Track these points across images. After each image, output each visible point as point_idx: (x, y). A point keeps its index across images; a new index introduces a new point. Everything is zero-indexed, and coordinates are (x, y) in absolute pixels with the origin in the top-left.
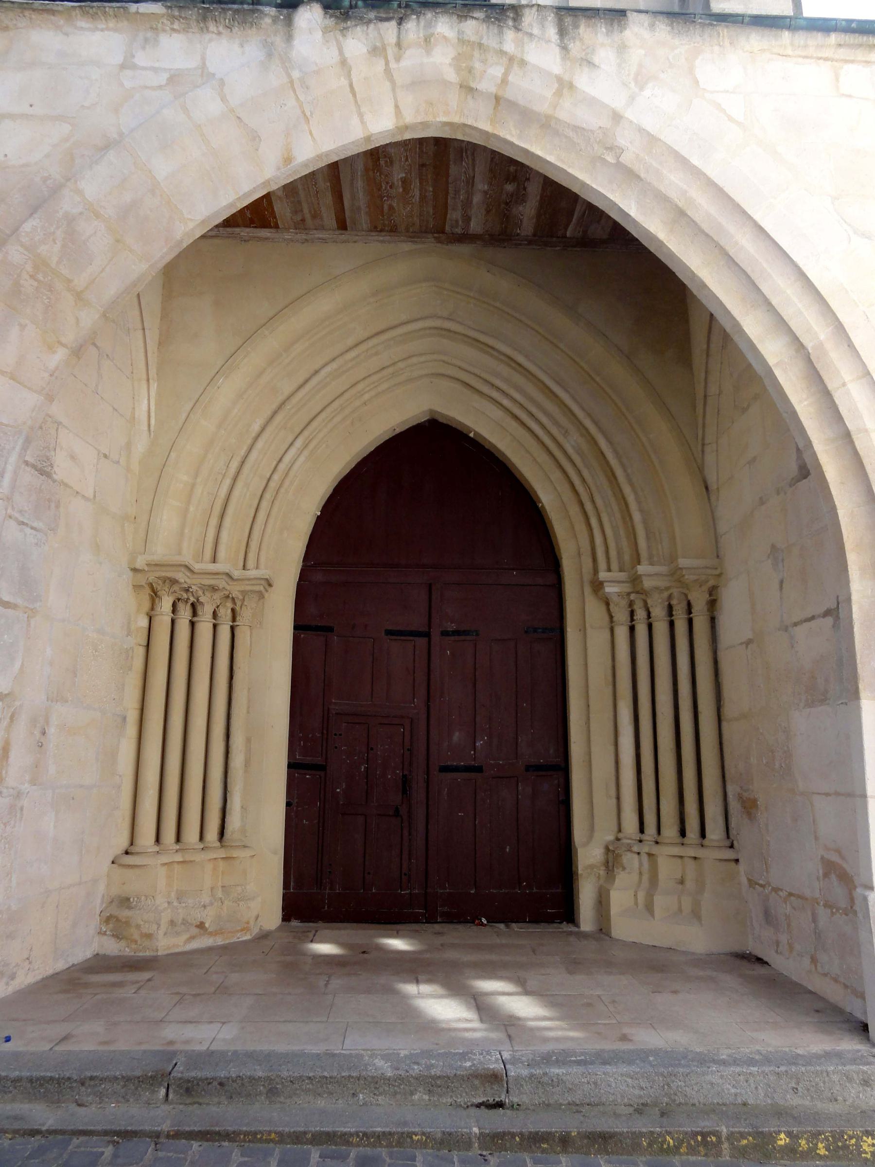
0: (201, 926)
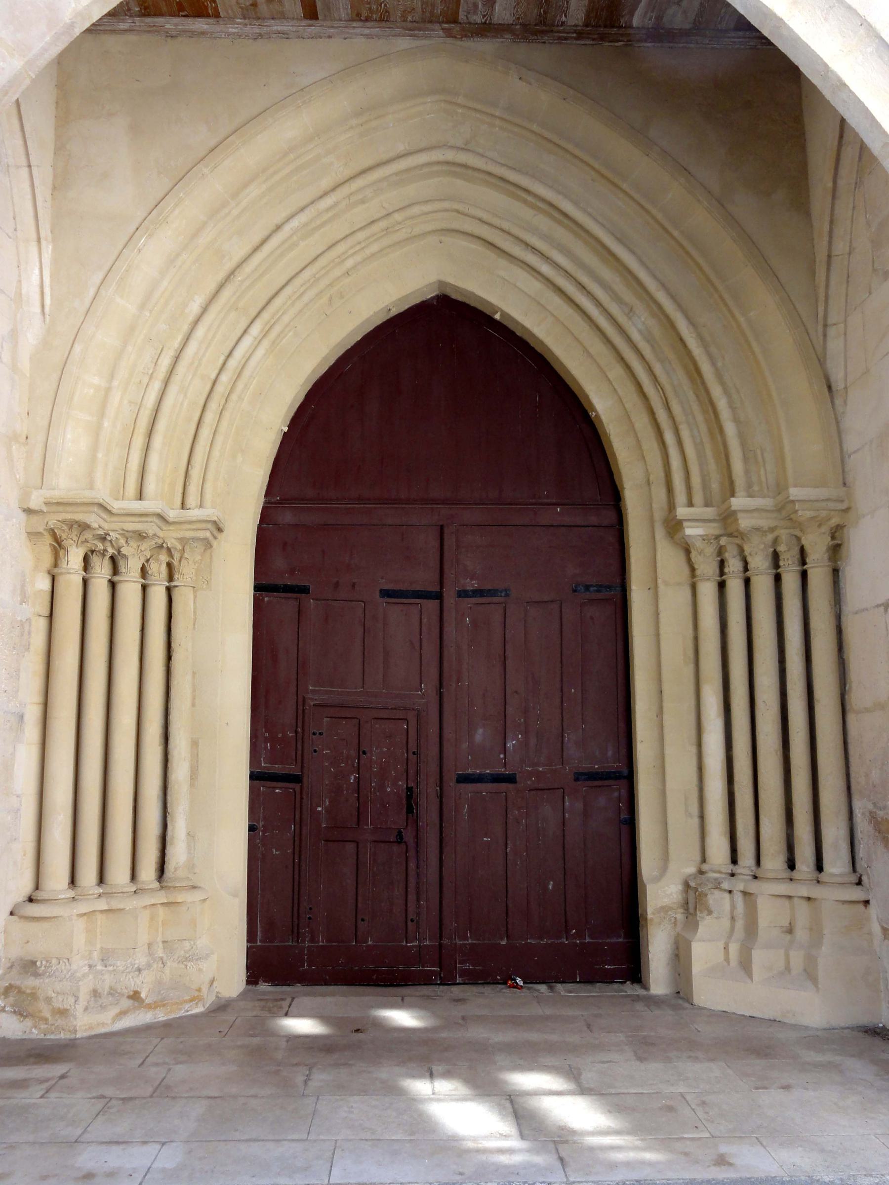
0: (135, 996)
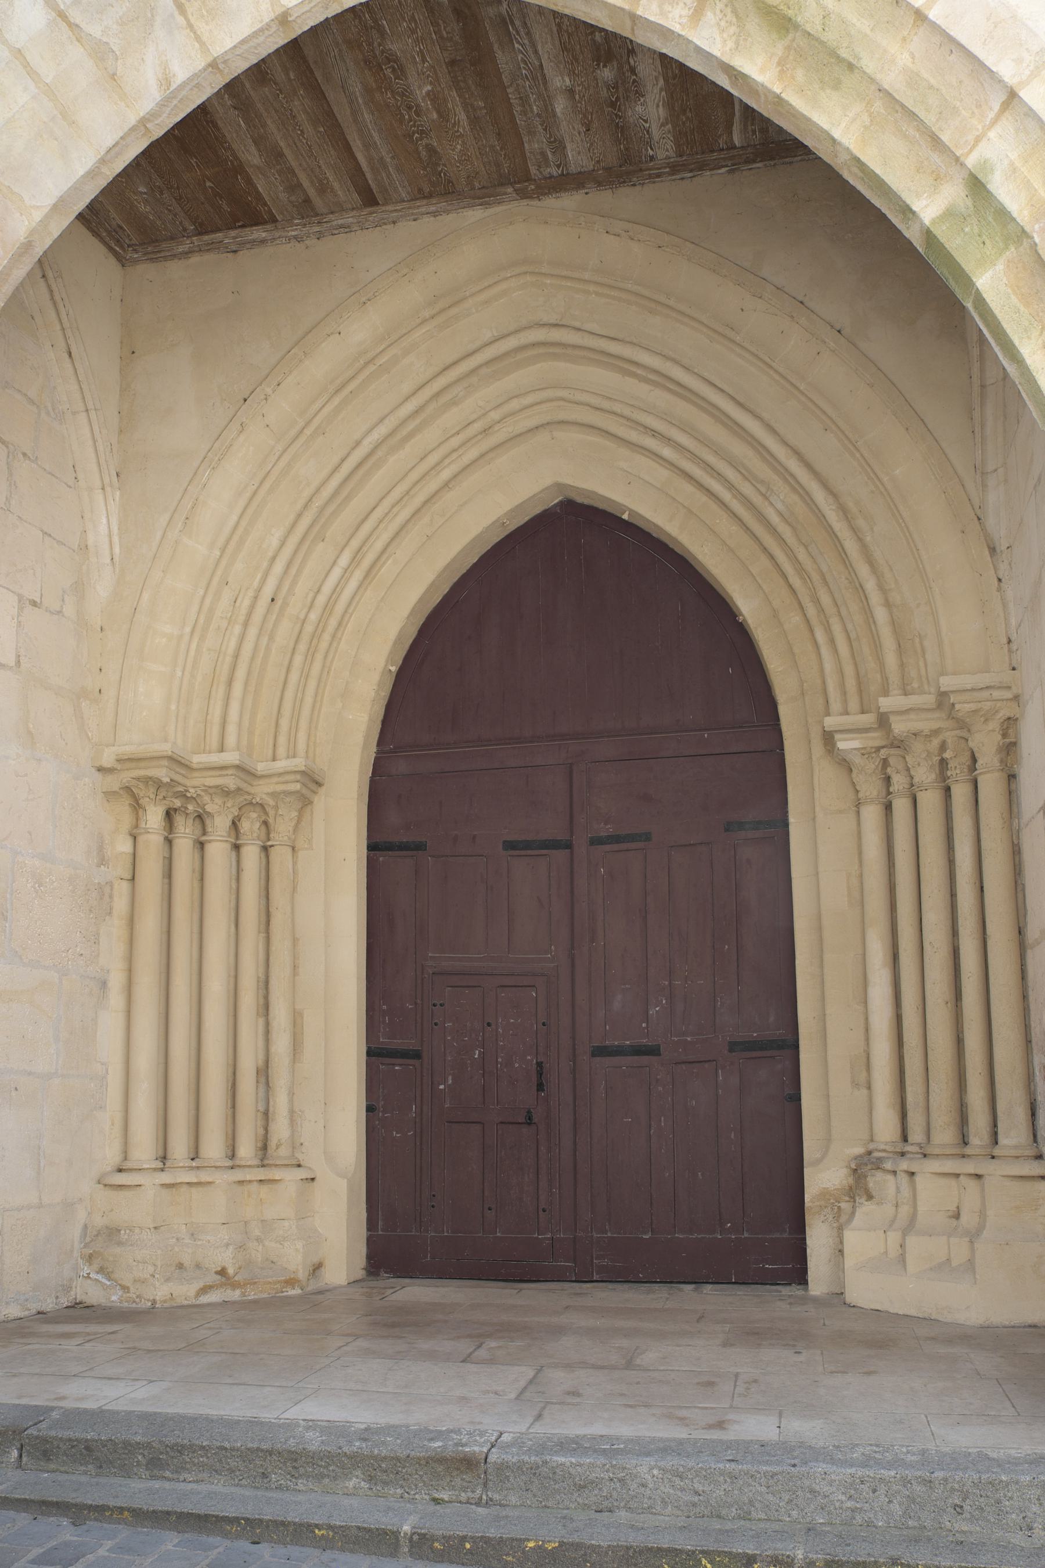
0: (222, 1272)
